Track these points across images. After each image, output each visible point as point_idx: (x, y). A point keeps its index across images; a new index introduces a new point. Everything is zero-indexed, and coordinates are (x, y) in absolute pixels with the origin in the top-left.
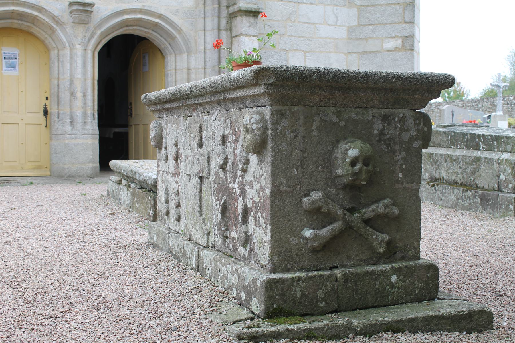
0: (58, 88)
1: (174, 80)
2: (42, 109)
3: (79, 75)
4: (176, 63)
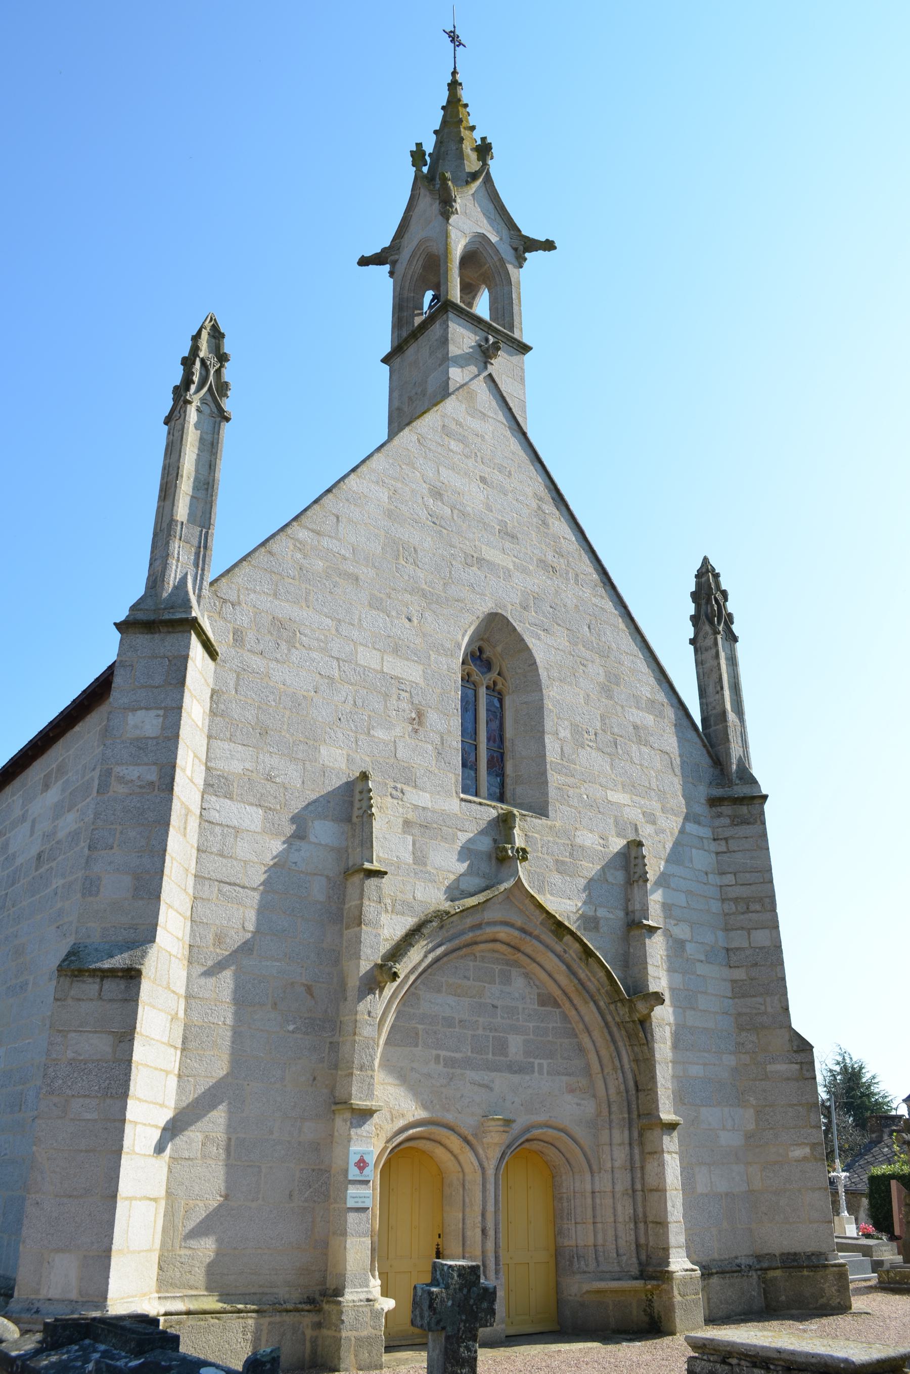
0: (463, 1224)
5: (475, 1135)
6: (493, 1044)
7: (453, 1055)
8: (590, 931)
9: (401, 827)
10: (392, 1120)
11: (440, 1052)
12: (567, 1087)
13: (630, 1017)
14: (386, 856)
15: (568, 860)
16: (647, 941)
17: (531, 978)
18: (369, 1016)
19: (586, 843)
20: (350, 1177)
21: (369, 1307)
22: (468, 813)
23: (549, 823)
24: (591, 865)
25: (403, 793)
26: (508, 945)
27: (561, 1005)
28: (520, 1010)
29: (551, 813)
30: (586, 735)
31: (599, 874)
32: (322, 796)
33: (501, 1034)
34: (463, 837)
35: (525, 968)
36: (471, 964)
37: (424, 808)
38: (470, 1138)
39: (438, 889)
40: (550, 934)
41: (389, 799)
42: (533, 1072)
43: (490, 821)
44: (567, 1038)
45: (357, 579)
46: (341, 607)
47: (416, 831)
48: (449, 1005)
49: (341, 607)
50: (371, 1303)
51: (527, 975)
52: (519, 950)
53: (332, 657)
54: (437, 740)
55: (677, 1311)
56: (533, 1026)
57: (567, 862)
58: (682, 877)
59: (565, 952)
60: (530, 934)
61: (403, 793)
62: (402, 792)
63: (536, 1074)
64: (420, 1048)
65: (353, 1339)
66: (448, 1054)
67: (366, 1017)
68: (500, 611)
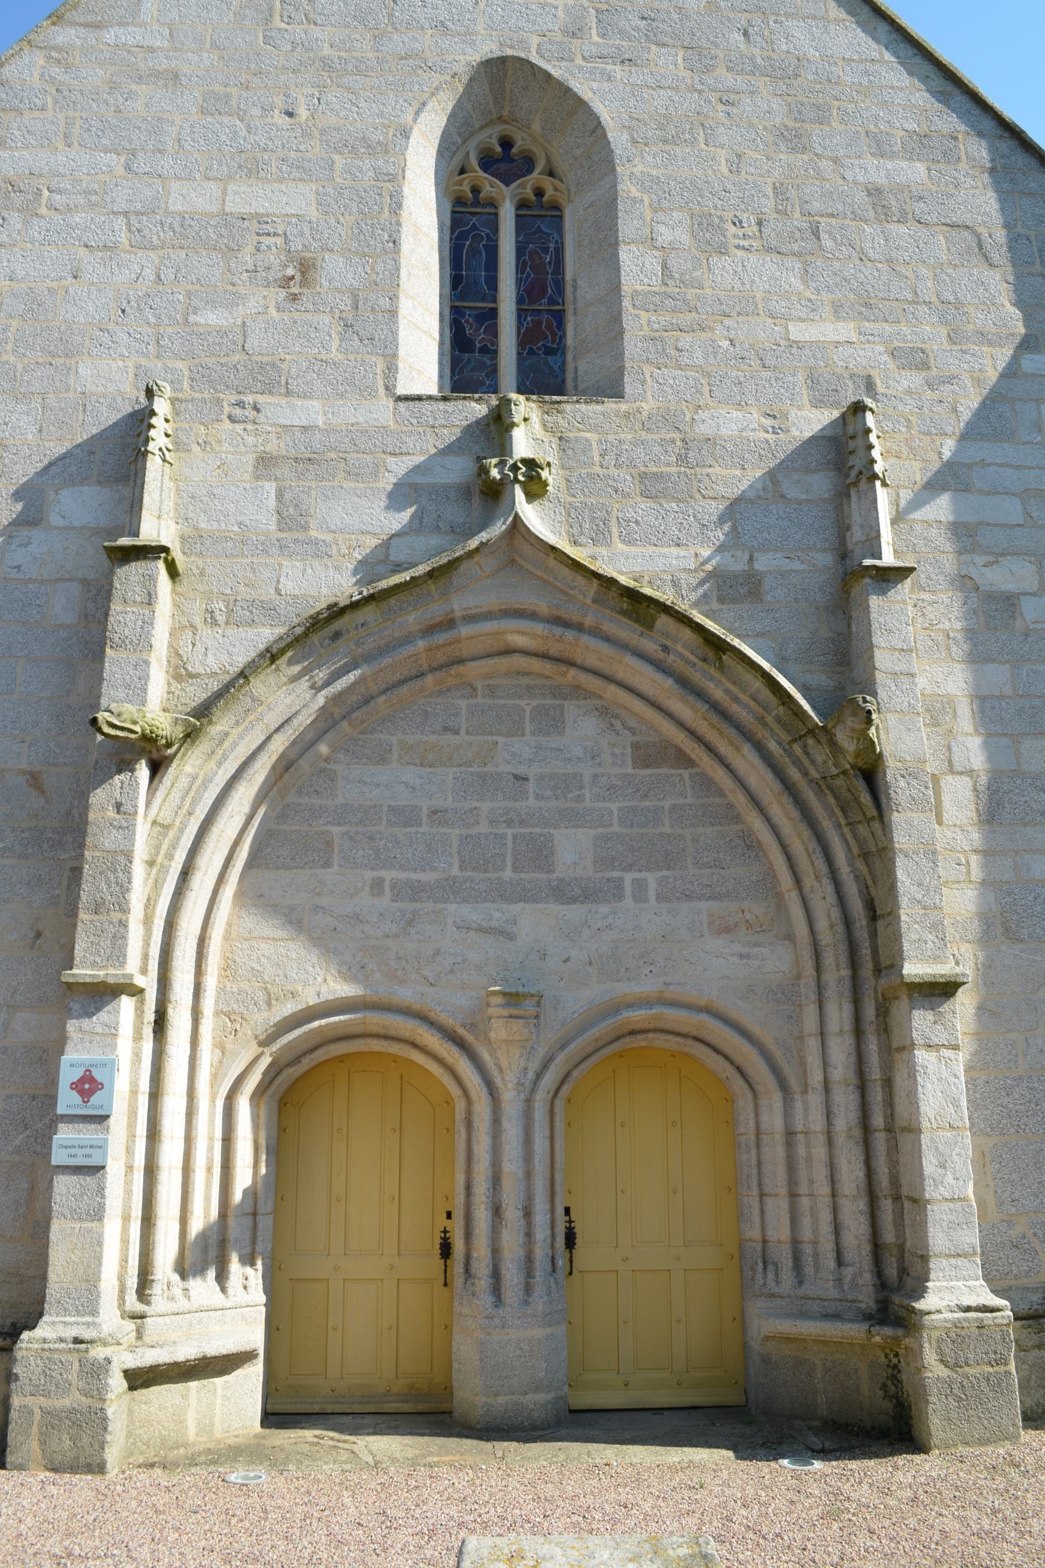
1: (754, 1162)
2: (438, 1241)
3: (511, 1166)
4: (757, 1115)
5: (472, 1027)
6: (514, 850)
7: (414, 876)
8: (734, 601)
9: (251, 469)
10: (269, 1005)
11: (383, 873)
12: (710, 924)
13: (836, 765)
14: (215, 526)
15: (673, 470)
16: (875, 602)
17: (616, 717)
18: (118, 812)
19: (724, 431)
20: (60, 1110)
21: (76, 1355)
22: (414, 421)
23: (623, 407)
24: (738, 472)
25: (258, 410)
26: (545, 656)
27: (696, 759)
28: (587, 780)
29: (630, 386)
30: (732, 229)
31: (759, 486)
32: (78, 446)
33: (538, 830)
34: (399, 467)
35: (600, 697)
36: (463, 703)
37: (305, 429)
38: (461, 1031)
39: (336, 568)
40: (624, 620)
41: (227, 425)
42: (620, 897)
43: (469, 426)
44: (712, 824)
45: (177, 76)
46: (139, 128)
47: (285, 471)
48: (406, 784)
49: (139, 128)
50: (83, 1346)
51: (604, 712)
52: (571, 663)
53: (114, 213)
54: (345, 303)
55: (932, 1399)
56: (620, 809)
57: (669, 475)
58: (1008, 465)
59: (666, 649)
60: (580, 628)
61: (258, 410)
62: (256, 408)
63: (628, 902)
64: (336, 868)
65: (37, 1412)
66: (404, 875)
67: (111, 813)
68: (509, 52)
